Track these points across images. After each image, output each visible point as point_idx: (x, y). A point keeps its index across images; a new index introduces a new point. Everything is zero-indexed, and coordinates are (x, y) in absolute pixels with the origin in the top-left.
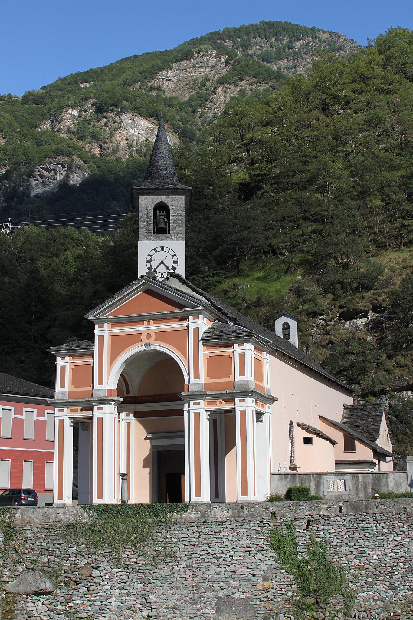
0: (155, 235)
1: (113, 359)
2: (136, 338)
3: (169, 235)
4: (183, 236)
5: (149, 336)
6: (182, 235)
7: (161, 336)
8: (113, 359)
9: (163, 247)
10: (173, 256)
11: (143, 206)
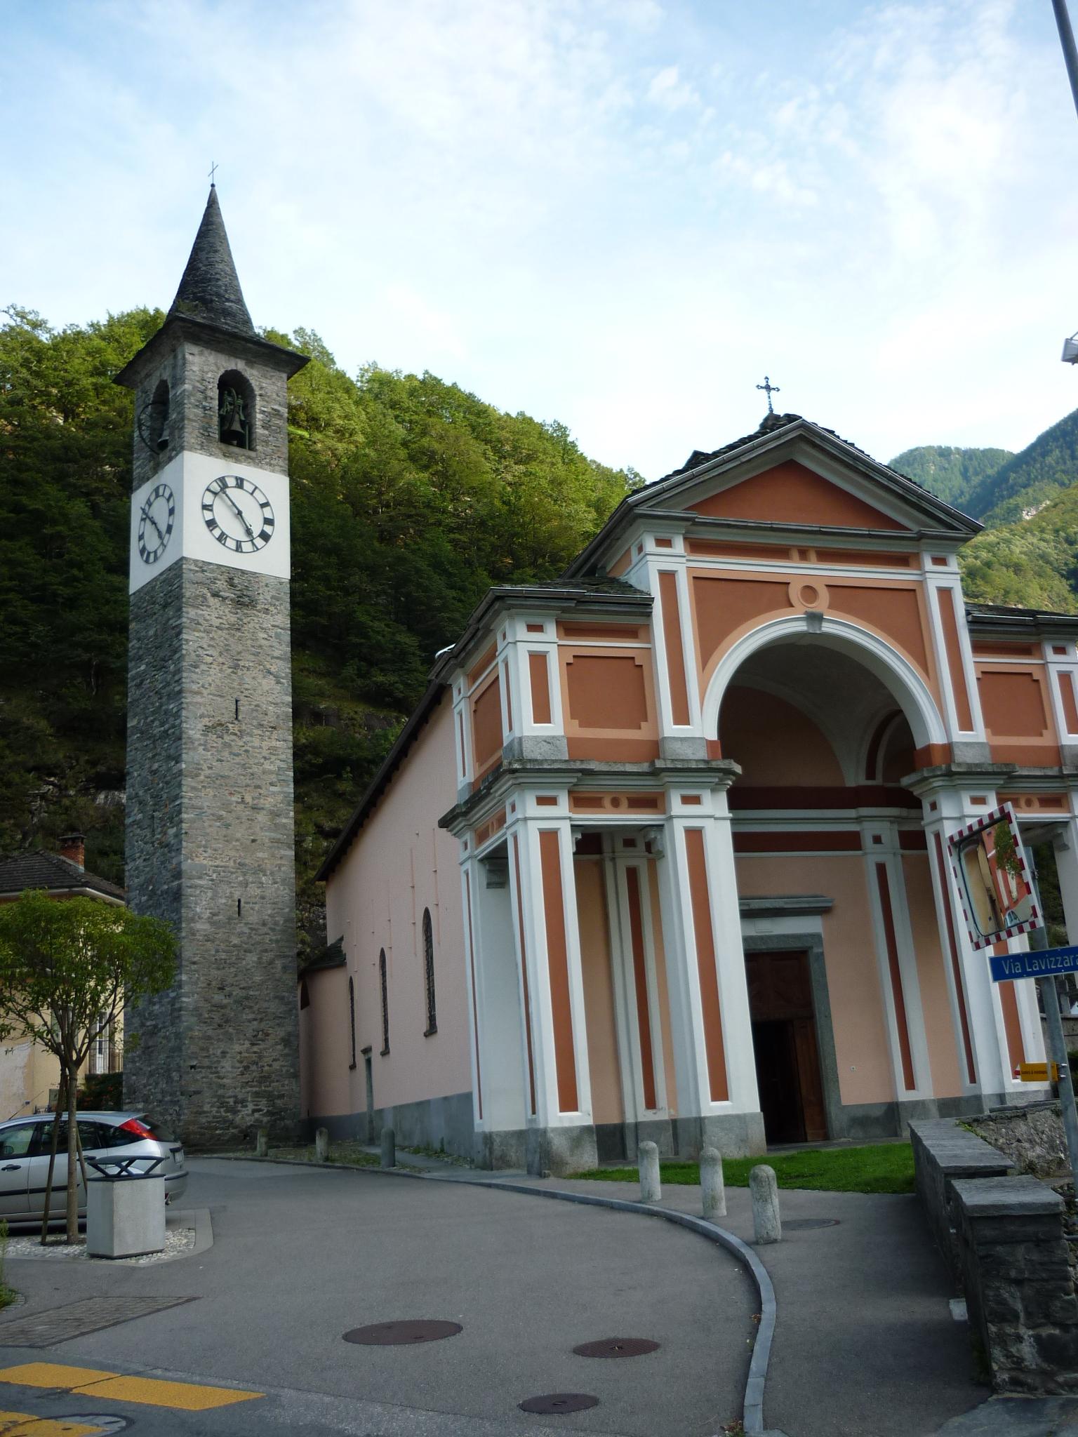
0: (223, 446)
1: (707, 652)
2: (774, 595)
3: (253, 454)
4: (284, 464)
5: (810, 592)
6: (281, 463)
7: (844, 595)
8: (707, 652)
9: (242, 480)
10: (264, 505)
11: (195, 369)
